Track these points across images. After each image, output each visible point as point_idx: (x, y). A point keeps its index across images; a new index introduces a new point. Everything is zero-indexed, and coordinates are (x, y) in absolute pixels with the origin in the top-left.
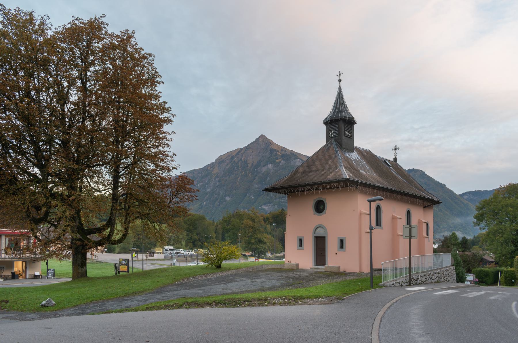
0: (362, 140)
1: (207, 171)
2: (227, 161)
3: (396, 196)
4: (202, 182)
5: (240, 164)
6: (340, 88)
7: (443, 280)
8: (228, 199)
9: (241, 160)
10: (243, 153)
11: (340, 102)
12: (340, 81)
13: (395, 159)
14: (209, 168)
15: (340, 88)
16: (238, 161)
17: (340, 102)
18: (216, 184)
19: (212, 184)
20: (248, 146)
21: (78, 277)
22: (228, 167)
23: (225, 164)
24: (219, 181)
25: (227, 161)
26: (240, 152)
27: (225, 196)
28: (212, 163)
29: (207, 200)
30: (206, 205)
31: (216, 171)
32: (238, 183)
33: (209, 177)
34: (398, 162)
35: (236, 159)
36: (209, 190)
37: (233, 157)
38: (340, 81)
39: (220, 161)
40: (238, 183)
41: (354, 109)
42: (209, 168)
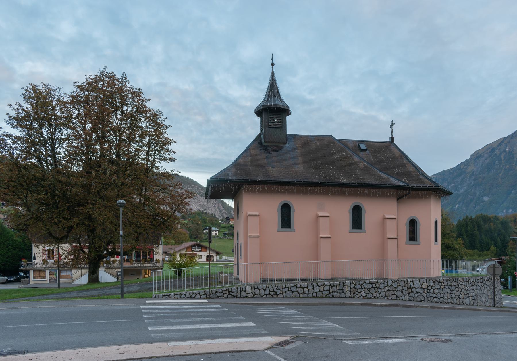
0: (294, 126)
1: (459, 171)
2: (486, 155)
3: (332, 189)
4: (454, 183)
5: (502, 157)
6: (273, 74)
7: (449, 301)
8: (486, 199)
9: (505, 151)
10: (508, 143)
11: (273, 90)
12: (273, 64)
13: (392, 138)
14: (462, 167)
15: (273, 74)
16: (501, 153)
17: (273, 90)
18: (471, 183)
19: (466, 183)
20: (514, 133)
21: (92, 282)
22: (486, 162)
23: (484, 158)
24: (475, 180)
25: (486, 155)
26: (503, 142)
27: (482, 196)
28: (467, 160)
29: (459, 202)
30: (458, 208)
31: (471, 168)
32: (500, 179)
33: (462, 176)
34: (395, 142)
35: (497, 152)
36: (462, 191)
37: (493, 150)
38: (273, 64)
39: (477, 156)
40: (500, 179)
41: (287, 94)
42: (462, 167)
